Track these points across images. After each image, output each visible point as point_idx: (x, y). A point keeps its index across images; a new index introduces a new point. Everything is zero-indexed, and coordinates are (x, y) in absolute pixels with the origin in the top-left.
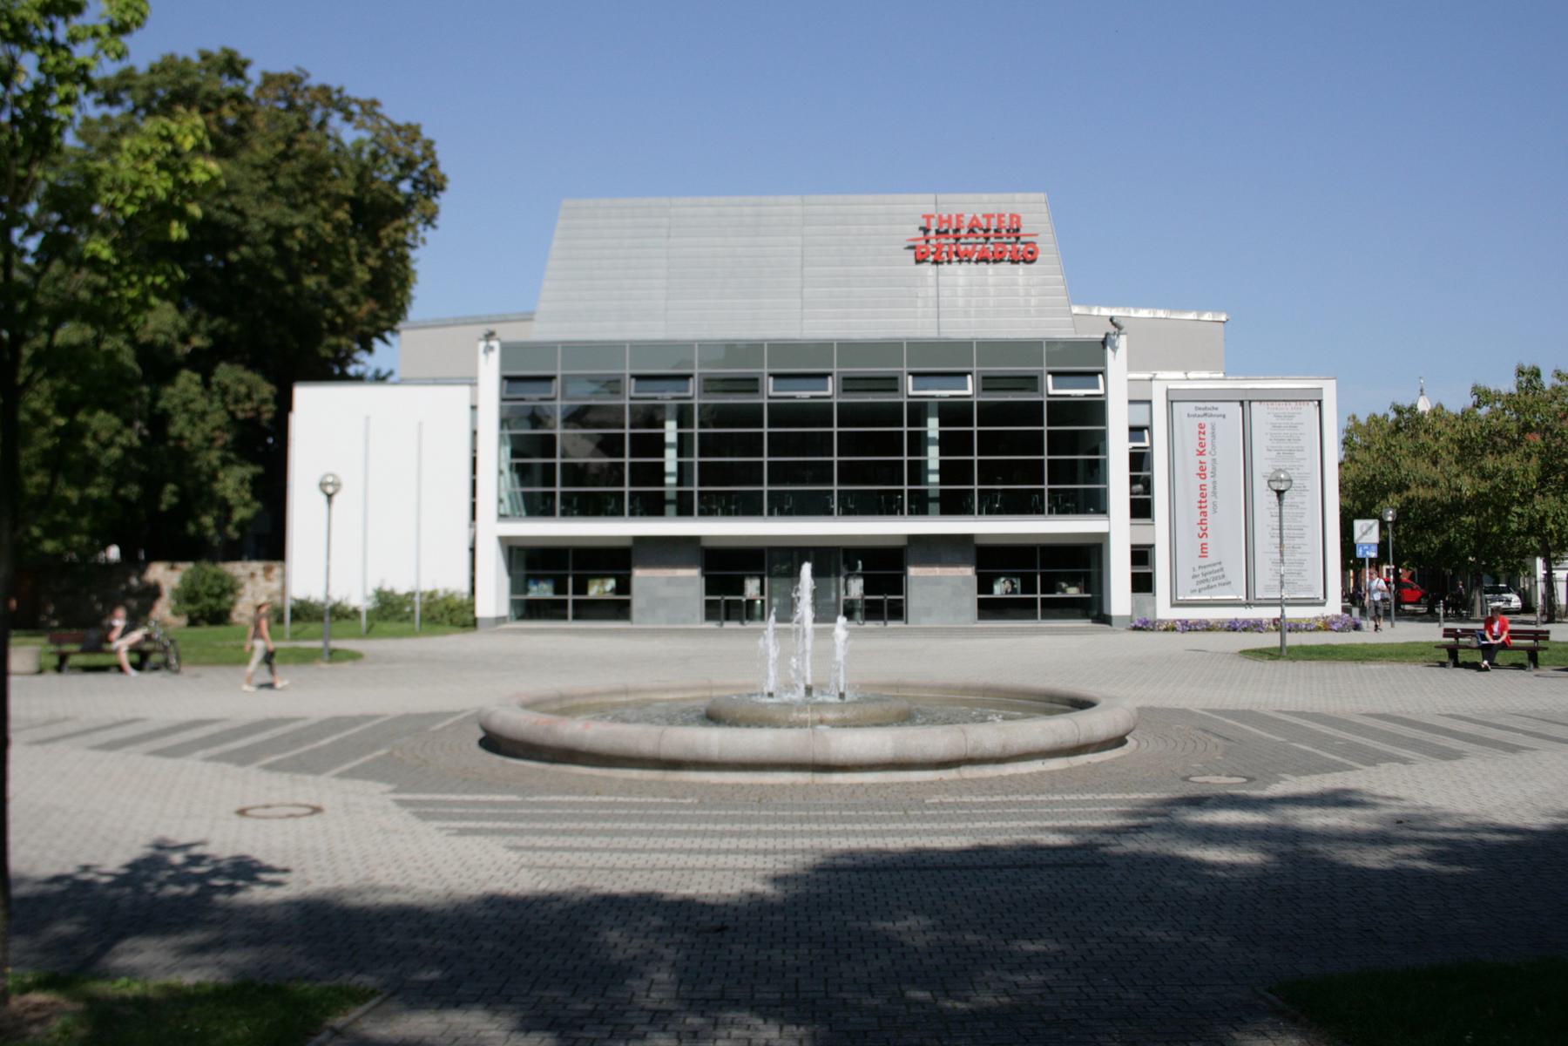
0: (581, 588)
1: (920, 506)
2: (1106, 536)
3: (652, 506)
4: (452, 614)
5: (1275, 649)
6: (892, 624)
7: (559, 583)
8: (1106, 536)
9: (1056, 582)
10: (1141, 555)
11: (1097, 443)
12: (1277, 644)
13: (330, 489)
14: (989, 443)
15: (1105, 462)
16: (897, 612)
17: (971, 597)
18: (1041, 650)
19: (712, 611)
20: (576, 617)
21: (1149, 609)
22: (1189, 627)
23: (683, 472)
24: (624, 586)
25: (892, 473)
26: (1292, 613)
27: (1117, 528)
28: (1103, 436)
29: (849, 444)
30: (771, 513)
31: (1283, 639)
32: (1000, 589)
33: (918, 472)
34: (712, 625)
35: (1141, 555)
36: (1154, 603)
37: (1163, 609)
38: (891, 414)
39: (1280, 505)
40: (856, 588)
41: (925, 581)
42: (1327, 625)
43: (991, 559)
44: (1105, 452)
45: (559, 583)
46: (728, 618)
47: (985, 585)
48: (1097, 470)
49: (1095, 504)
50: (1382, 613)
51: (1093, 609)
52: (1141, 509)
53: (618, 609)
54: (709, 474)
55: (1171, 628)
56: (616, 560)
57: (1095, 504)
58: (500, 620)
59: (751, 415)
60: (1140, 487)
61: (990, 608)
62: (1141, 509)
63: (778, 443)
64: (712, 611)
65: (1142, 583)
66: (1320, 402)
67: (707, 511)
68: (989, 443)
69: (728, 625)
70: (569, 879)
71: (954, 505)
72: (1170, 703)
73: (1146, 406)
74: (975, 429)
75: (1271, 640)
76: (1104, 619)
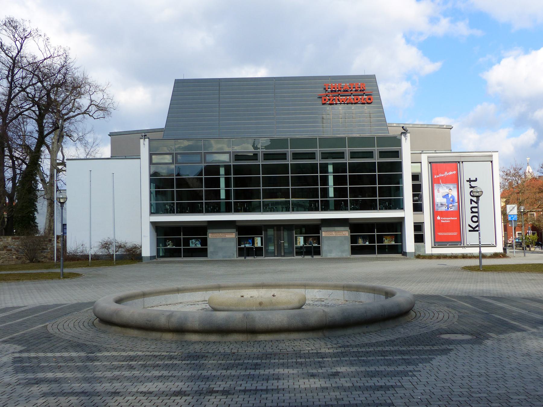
0: (187, 243)
1: (326, 207)
2: (403, 219)
3: (215, 209)
4: (132, 256)
5: (477, 266)
6: (316, 257)
7: (177, 243)
8: (403, 219)
9: (378, 239)
10: (418, 227)
11: (398, 179)
12: (478, 264)
13: (62, 201)
14: (354, 180)
15: (402, 187)
16: (317, 251)
17: (348, 246)
18: (375, 269)
19: (242, 252)
20: (379, 253)
21: (422, 250)
22: (439, 257)
23: (228, 193)
24: (204, 242)
25: (314, 193)
26: (484, 250)
27: (408, 214)
28: (401, 176)
29: (297, 181)
30: (293, 210)
31: (480, 262)
32: (361, 242)
33: (325, 192)
34: (243, 258)
35: (418, 227)
36: (424, 247)
37: (428, 248)
38: (313, 168)
39: (62, 209)
40: (301, 241)
41: (329, 238)
42: (496, 256)
43: (356, 227)
44: (402, 184)
45: (177, 243)
46: (248, 255)
47: (354, 239)
48: (399, 191)
49: (398, 205)
50: (162, 257)
51: (398, 249)
52: (418, 208)
53: (202, 252)
54: (238, 195)
55: (431, 257)
56: (200, 230)
57: (398, 205)
58: (152, 258)
59: (255, 169)
60: (417, 198)
61: (356, 250)
62: (418, 208)
63: (285, 181)
64: (242, 252)
65: (419, 239)
66: (492, 162)
67: (237, 211)
68: (354, 180)
69: (248, 258)
70: (180, 386)
71: (338, 207)
72: (431, 292)
73: (419, 164)
74: (348, 174)
75: (475, 262)
76: (405, 254)
